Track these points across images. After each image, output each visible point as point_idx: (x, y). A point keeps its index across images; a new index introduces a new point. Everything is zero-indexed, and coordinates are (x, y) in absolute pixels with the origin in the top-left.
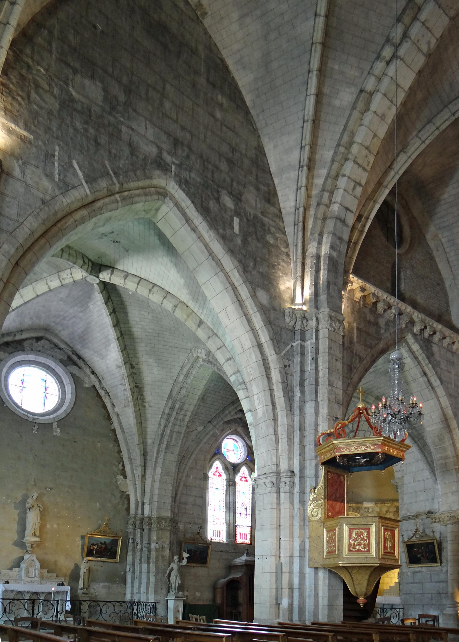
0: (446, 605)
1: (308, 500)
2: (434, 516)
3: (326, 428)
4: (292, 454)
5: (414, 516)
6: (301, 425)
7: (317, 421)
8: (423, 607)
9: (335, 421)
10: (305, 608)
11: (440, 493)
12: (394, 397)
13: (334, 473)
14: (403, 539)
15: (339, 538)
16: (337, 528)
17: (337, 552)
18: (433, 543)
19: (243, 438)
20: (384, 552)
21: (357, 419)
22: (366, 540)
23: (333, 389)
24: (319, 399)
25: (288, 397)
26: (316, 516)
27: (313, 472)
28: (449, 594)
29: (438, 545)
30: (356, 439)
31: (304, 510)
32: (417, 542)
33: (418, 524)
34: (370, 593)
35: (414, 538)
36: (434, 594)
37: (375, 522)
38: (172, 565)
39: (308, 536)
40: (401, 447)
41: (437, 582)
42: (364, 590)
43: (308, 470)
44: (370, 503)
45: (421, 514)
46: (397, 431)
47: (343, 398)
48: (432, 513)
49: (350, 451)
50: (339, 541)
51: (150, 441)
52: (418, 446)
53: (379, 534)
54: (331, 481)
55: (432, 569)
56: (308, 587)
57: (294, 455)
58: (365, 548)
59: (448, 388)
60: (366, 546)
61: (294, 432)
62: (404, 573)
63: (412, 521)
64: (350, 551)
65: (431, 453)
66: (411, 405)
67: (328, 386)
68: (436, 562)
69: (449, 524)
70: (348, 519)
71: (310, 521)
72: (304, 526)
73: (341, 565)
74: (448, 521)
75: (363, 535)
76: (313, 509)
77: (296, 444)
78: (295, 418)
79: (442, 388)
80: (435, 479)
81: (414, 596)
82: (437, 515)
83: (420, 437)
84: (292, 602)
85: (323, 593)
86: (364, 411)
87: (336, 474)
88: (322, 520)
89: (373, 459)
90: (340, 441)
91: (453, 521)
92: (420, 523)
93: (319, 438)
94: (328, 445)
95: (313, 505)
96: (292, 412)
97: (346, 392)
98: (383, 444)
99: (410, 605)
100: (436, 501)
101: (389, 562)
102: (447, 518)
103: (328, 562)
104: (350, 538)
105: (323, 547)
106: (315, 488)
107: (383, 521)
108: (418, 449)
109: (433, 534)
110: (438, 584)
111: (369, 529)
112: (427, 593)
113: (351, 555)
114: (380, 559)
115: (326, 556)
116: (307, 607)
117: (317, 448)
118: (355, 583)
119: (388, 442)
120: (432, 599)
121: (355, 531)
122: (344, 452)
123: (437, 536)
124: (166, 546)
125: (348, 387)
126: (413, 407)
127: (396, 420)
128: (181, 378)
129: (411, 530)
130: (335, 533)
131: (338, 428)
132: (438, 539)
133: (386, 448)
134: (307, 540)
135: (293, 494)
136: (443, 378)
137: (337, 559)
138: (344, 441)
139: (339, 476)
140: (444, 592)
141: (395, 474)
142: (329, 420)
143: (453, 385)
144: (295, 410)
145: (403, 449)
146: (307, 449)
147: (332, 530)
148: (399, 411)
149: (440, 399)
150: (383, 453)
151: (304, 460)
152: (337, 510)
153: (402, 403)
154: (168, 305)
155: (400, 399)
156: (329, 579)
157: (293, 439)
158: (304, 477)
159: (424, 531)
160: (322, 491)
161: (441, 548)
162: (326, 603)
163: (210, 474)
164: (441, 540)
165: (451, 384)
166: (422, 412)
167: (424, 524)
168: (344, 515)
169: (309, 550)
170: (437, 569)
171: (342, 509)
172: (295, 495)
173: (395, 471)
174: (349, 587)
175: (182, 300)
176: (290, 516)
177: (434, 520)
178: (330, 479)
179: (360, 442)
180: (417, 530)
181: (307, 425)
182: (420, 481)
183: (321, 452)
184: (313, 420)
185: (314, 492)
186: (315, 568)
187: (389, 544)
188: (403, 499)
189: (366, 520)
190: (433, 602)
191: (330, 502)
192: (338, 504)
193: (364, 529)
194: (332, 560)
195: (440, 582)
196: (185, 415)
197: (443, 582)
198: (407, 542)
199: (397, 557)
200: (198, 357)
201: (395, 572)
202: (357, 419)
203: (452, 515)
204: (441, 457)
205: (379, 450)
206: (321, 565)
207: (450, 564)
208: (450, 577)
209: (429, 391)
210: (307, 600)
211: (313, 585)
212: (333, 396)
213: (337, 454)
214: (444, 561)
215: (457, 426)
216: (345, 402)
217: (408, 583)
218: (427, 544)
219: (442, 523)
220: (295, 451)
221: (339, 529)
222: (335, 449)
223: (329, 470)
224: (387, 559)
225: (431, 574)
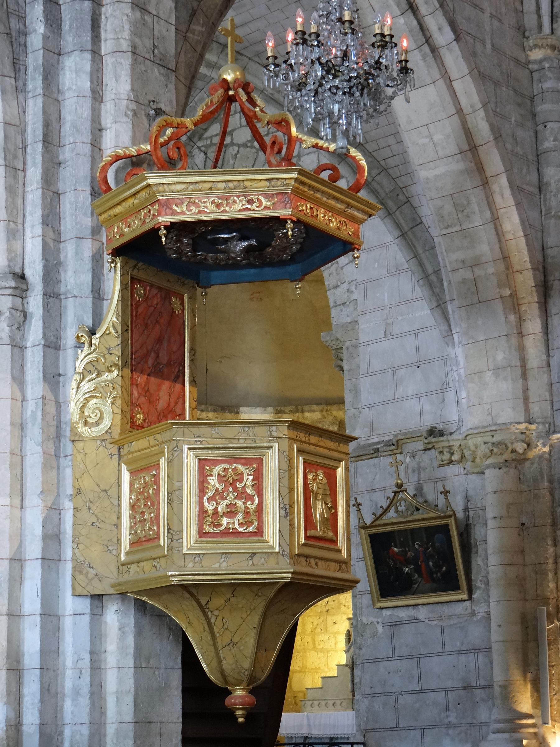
0: (487, 724)
1: (70, 371)
2: (446, 444)
3: (126, 138)
4: (20, 220)
5: (389, 444)
6: (47, 125)
7: (99, 116)
8: (423, 735)
9: (151, 119)
10: (61, 733)
11: (462, 371)
12: (329, 13)
13: (152, 286)
14: (361, 518)
15: (170, 493)
16: (162, 461)
17: (163, 540)
18: (447, 526)
20: (307, 537)
21: (215, 129)
22: (251, 498)
23: (148, 18)
24: (106, 47)
25: (9, 34)
26: (97, 424)
27: (87, 278)
28: (497, 690)
29: (460, 535)
30: (217, 174)
31: (58, 404)
32: (401, 527)
33: (402, 468)
34: (267, 672)
35: (392, 513)
36: (453, 689)
37: (277, 439)
39: (70, 491)
40: (349, 205)
41: (460, 652)
42: (247, 664)
43: (70, 273)
44: (258, 409)
45: (412, 437)
46: (340, 118)
47: (177, 55)
48: (441, 434)
49: (200, 212)
50: (170, 502)
52: (398, 226)
53: (291, 477)
54: (141, 309)
55: (446, 610)
56: (69, 662)
57: (27, 225)
58: (248, 523)
59: (474, 54)
60: (253, 516)
61: (25, 148)
62: (365, 625)
63: (385, 461)
64: (202, 534)
65: (433, 248)
66: (378, 38)
67: (133, 9)
68: (454, 586)
69: (488, 467)
70: (195, 430)
71: (76, 439)
72: (57, 456)
73: (175, 580)
74: (486, 457)
75: (241, 481)
76: (87, 400)
77: (34, 187)
78: (30, 102)
79: (459, 52)
80: (445, 327)
81: (396, 701)
82: (455, 441)
83: (401, 197)
84: (19, 715)
85: (120, 681)
86: (240, 90)
87: (160, 289)
89: (270, 245)
90: (171, 180)
91: (501, 459)
92: (407, 465)
93: (104, 169)
94: (132, 191)
95: (86, 386)
96: (20, 84)
97: (185, 38)
99: (385, 729)
100: (450, 396)
101: (322, 570)
102: (483, 449)
103: (134, 573)
104: (202, 491)
105: (118, 526)
106: (92, 332)
107: (302, 435)
108: (397, 233)
109: (447, 498)
110: (463, 658)
111: (260, 461)
112: (435, 691)
113: (208, 547)
114: (295, 558)
115: (127, 554)
116: (67, 732)
117: (98, 201)
118: (219, 640)
119: (310, 186)
120: (447, 709)
121: (218, 469)
122: (183, 213)
123: (458, 504)
125: (190, 21)
126: (384, 46)
127: (337, 82)
129: (384, 489)
130: (157, 477)
131: (161, 140)
132: (460, 515)
133: (305, 207)
134: (68, 505)
135: (22, 349)
136: (463, 25)
137: (163, 560)
138: (182, 179)
139: (167, 294)
140: (483, 683)
141: (334, 313)
142: (135, 114)
143: (489, 46)
144: (29, 77)
145: (356, 213)
146: (68, 205)
147: (146, 469)
148: (345, 55)
149: (455, 84)
150: (298, 223)
151: (58, 240)
152: (161, 405)
153: (353, 31)
155: (347, 17)
156: (139, 632)
157: (24, 171)
158: (57, 296)
159: (419, 489)
160: (115, 342)
161: (470, 544)
162: (128, 715)
164: (467, 518)
165: (483, 42)
166: (409, 65)
167: (419, 470)
168: (185, 419)
169: (74, 537)
170: (459, 609)
171: (176, 403)
172: (29, 353)
173: (332, 304)
174: (200, 657)
176: (13, 424)
177: (446, 456)
178: (138, 304)
179: (231, 185)
180: (399, 486)
181: (67, 128)
182: (402, 335)
183: (111, 212)
184: (86, 112)
185: (90, 344)
186: (93, 597)
187: (319, 509)
188: (356, 390)
189: (251, 431)
190: (453, 718)
191: (141, 379)
192: (166, 385)
193: (246, 462)
194: (146, 566)
195: (468, 652)
197: (477, 650)
198: (372, 526)
199: (344, 554)
201: (337, 633)
202: (215, 129)
203: (497, 438)
204: (463, 261)
205: (284, 212)
206: (113, 586)
207: (495, 594)
208: (496, 636)
209: (424, 59)
210: (68, 705)
211: (87, 657)
212: (148, 43)
213: (161, 219)
214: (479, 584)
215: (501, 168)
216: (182, 66)
217: (376, 661)
218: (431, 531)
219: (469, 464)
220: (29, 208)
221: (169, 461)
222: (152, 204)
223: (135, 272)
224: (315, 558)
225: (442, 627)
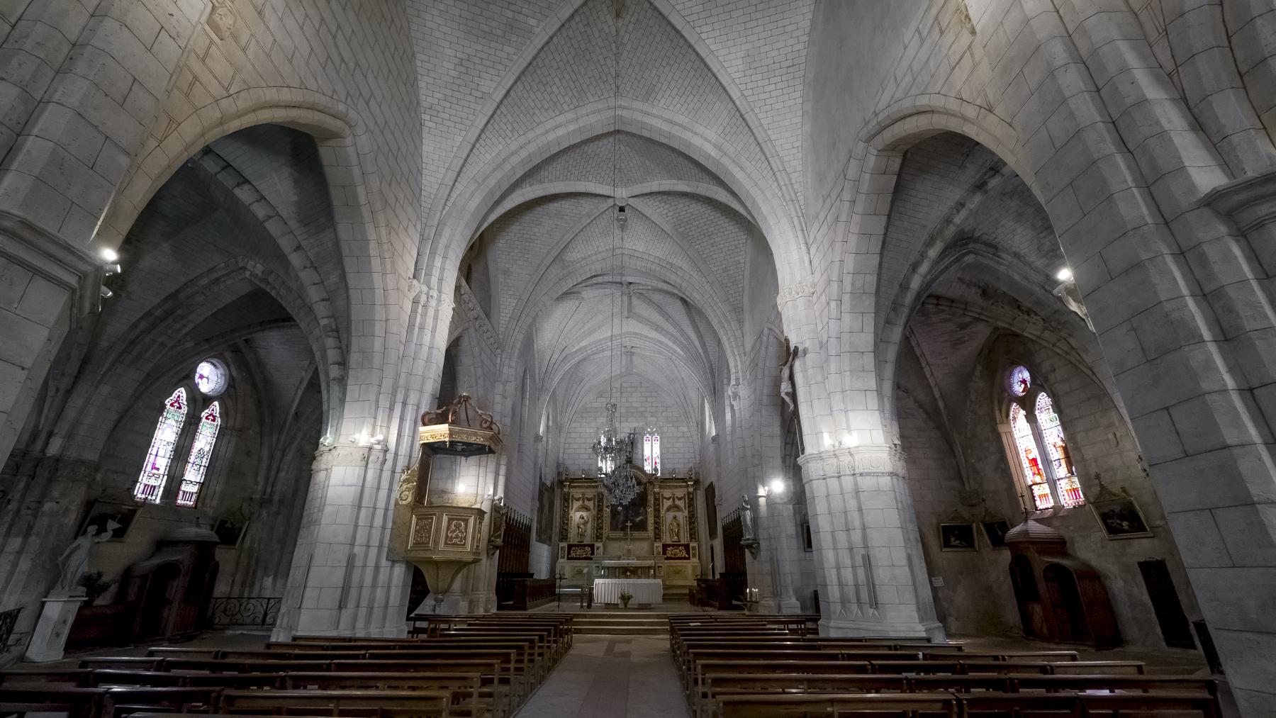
19: (228, 366)
38: (81, 540)
51: (104, 344)
64: (446, 543)
88: (412, 504)
98: (491, 438)
103: (413, 554)
104: (448, 528)
111: (467, 520)
124: (73, 508)
128: (204, 281)
130: (431, 523)
154: (260, 211)
163: (168, 402)
175: (281, 213)
196: (184, 326)
200: (244, 268)
